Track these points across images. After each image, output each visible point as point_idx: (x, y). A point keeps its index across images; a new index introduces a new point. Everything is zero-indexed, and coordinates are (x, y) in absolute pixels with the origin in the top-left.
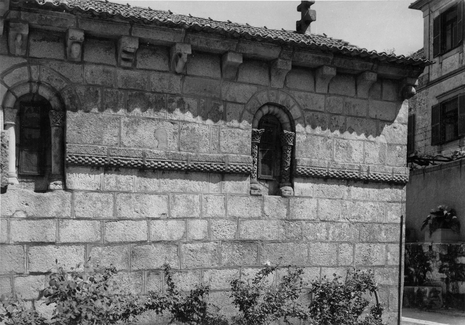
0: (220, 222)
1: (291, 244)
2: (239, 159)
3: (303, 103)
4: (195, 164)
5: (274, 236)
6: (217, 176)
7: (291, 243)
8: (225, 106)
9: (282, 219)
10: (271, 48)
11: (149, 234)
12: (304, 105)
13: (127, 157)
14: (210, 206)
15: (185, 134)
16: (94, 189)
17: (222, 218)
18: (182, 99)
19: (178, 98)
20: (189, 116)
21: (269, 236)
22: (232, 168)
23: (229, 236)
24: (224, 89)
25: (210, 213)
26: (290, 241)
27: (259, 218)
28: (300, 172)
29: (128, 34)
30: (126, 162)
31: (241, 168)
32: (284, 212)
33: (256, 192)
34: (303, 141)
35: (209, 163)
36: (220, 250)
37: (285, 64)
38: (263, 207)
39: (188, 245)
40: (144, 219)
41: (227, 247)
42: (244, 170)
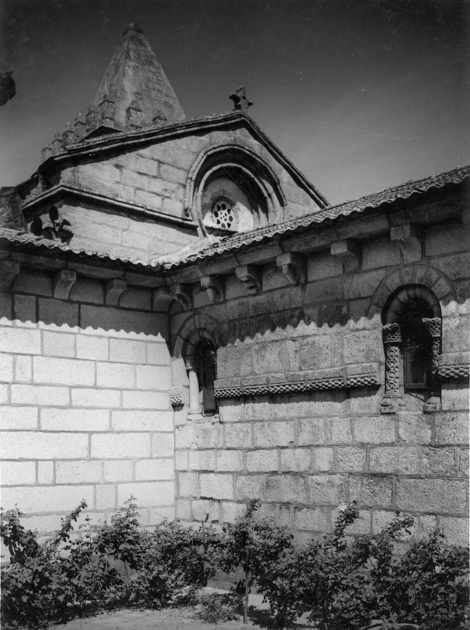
0: (347, 449)
1: (440, 481)
2: (359, 370)
3: (453, 272)
4: (313, 383)
5: (413, 469)
6: (341, 394)
7: (438, 480)
8: (348, 306)
9: (424, 445)
10: (372, 220)
11: (280, 464)
12: (454, 275)
13: (255, 385)
14: (335, 430)
15: (306, 350)
16: (237, 420)
17: (347, 445)
18: (302, 311)
19: (298, 312)
20: (312, 328)
21: (406, 469)
22: (352, 382)
23: (357, 467)
24: (346, 286)
25: (335, 440)
26: (438, 477)
27: (392, 444)
28: (443, 375)
29: (238, 264)
30: (255, 391)
31: (362, 380)
32: (427, 435)
33: (387, 410)
34: (453, 328)
35: (326, 380)
36: (347, 485)
37: (400, 231)
38: (397, 429)
39: (315, 477)
40: (276, 448)
41: (355, 481)
42: (366, 383)
